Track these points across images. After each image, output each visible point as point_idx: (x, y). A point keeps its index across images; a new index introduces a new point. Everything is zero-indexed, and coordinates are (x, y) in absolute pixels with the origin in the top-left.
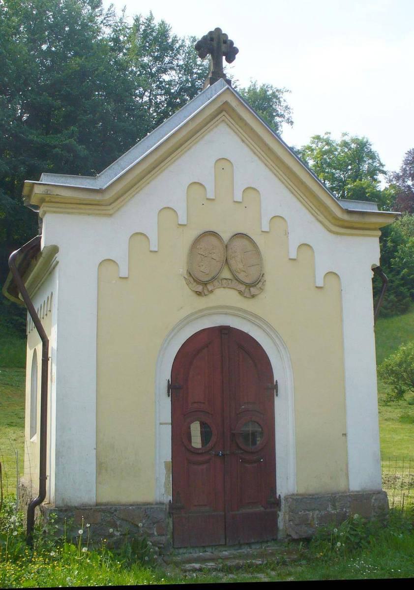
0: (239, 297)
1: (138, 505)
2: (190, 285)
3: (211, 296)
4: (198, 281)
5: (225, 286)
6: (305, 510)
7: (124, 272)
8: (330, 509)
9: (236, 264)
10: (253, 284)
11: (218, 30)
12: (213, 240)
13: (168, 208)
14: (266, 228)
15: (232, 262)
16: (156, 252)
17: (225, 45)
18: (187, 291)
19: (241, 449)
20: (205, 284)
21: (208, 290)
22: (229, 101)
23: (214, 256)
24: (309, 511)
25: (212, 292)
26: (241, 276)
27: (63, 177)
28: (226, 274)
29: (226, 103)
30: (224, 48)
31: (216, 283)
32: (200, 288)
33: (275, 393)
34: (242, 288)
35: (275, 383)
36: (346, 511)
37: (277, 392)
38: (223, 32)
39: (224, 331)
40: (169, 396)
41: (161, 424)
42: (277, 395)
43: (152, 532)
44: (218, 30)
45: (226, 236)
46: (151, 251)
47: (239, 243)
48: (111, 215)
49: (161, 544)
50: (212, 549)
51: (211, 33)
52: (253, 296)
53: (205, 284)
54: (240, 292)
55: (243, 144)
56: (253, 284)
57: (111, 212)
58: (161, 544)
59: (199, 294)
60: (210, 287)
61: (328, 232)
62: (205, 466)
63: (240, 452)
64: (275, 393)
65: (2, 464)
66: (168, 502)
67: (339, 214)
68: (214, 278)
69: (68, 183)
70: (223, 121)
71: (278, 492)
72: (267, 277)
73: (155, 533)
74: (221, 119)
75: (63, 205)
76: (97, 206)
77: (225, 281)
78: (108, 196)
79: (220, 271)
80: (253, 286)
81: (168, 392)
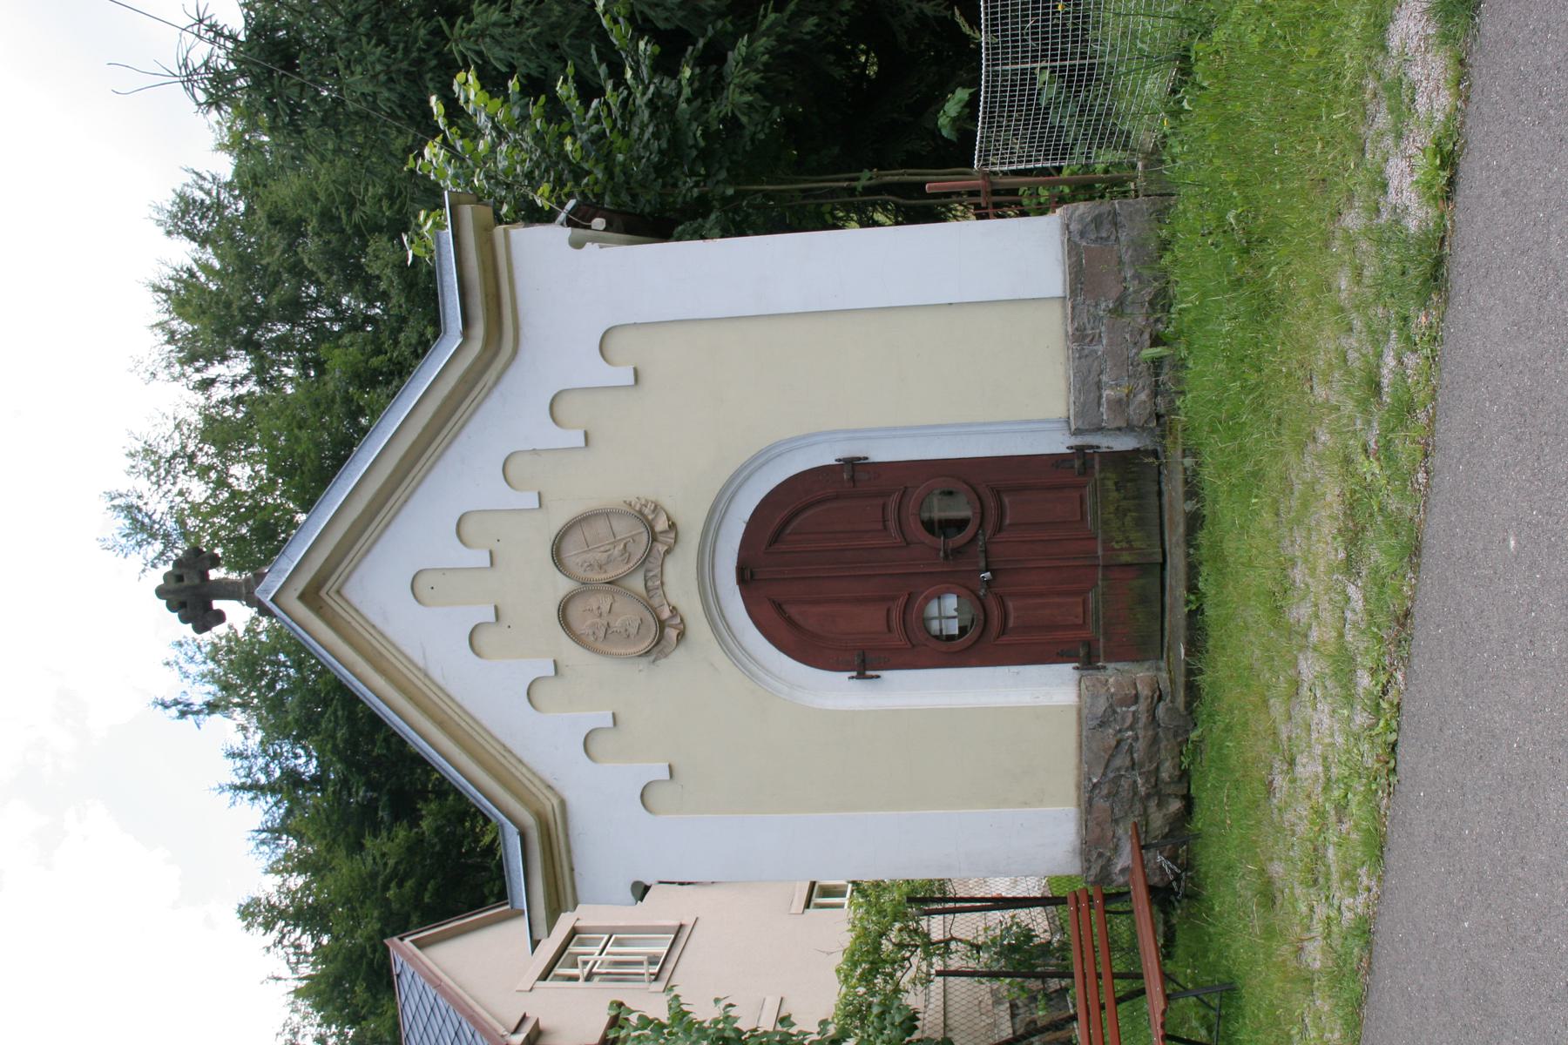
6: (1099, 404)
8: (1100, 349)
11: (161, 592)
12: (575, 612)
13: (528, 694)
17: (185, 579)
18: (679, 657)
19: (976, 534)
22: (297, 593)
23: (605, 608)
24: (1100, 397)
25: (674, 610)
26: (638, 551)
28: (637, 583)
29: (302, 597)
30: (191, 580)
31: (656, 602)
32: (672, 633)
36: (1104, 311)
37: (859, 459)
38: (162, 582)
39: (746, 576)
40: (878, 677)
42: (867, 458)
43: (1130, 715)
44: (161, 592)
45: (565, 586)
48: (563, 803)
50: (1140, 815)
51: (171, 608)
52: (672, 526)
53: (662, 625)
57: (555, 802)
59: (681, 635)
60: (666, 614)
61: (516, 364)
62: (1010, 605)
63: (981, 537)
65: (991, 1041)
66: (1076, 671)
70: (338, 592)
71: (1063, 450)
73: (1133, 708)
74: (336, 598)
75: (560, 883)
77: (650, 584)
78: (529, 820)
80: (652, 528)
81: (872, 677)
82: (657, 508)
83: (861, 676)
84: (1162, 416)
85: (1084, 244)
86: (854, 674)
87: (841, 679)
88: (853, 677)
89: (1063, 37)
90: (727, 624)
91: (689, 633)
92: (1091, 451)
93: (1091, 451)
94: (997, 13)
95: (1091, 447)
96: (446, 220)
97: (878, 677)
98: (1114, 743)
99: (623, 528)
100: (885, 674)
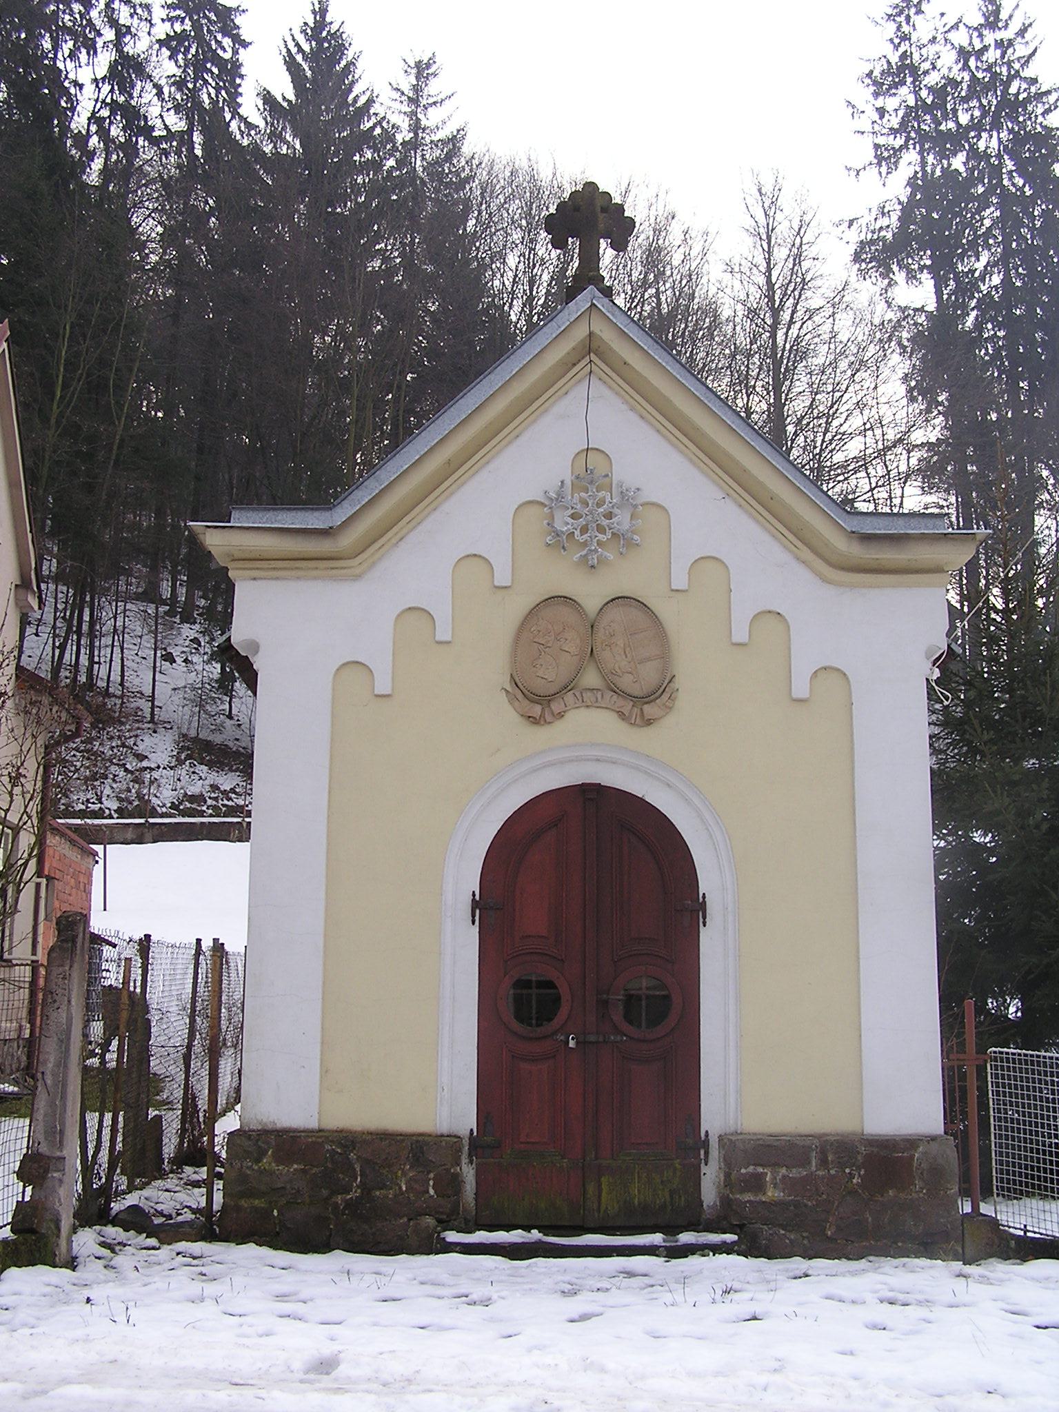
0: (622, 726)
1: (377, 1134)
2: (517, 703)
3: (559, 726)
4: (534, 697)
5: (590, 704)
7: (383, 686)
9: (613, 658)
10: (649, 697)
11: (591, 186)
12: (565, 613)
14: (680, 581)
15: (605, 655)
16: (448, 643)
18: (510, 715)
20: (544, 700)
21: (553, 714)
25: (561, 715)
26: (626, 682)
27: (269, 510)
32: (537, 710)
33: (701, 920)
34: (627, 706)
35: (701, 900)
37: (704, 918)
40: (473, 923)
41: (105, 910)
46: (438, 643)
47: (617, 614)
49: (442, 1213)
52: (649, 722)
54: (621, 715)
55: (259, 582)
56: (649, 697)
57: (357, 571)
58: (442, 1213)
60: (556, 706)
64: (701, 920)
66: (468, 1133)
67: (840, 544)
68: (566, 688)
69: (279, 522)
72: (677, 684)
76: (331, 561)
77: (589, 694)
78: (346, 541)
79: (579, 671)
81: (473, 916)
82: (669, 708)
83: (475, 904)
84: (741, 1230)
85: (917, 1155)
86: (477, 897)
87: (472, 883)
88: (474, 894)
89: (1026, 1166)
90: (538, 769)
91: (535, 729)
92: (702, 1157)
93: (702, 1157)
94: (1023, 1099)
95: (707, 1153)
96: (583, 307)
97: (473, 923)
98: (279, 1185)
99: (649, 676)
100: (476, 929)
